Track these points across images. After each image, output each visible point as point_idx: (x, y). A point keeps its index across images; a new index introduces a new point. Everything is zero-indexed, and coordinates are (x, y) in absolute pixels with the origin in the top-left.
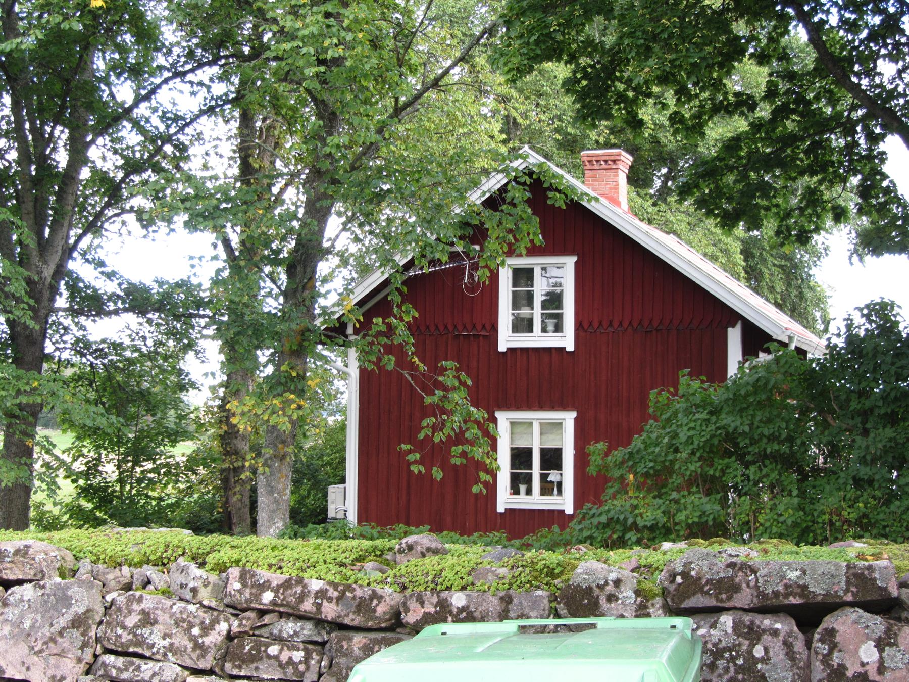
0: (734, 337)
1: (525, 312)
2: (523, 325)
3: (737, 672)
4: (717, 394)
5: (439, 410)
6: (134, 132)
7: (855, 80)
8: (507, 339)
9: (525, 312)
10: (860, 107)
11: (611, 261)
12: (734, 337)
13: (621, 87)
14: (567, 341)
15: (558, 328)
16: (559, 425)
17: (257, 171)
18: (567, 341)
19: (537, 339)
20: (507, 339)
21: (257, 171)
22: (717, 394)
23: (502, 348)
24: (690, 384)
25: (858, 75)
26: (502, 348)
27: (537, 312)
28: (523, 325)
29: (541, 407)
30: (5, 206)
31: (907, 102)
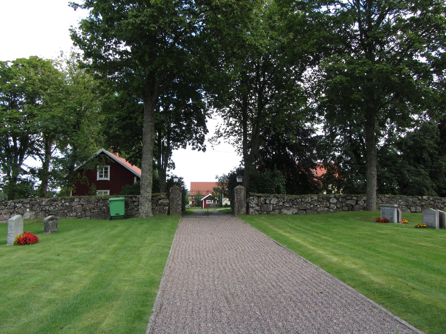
0: (135, 178)
2: (101, 176)
5: (91, 190)
8: (98, 178)
10: (249, 108)
12: (135, 178)
13: (322, 118)
15: (107, 177)
16: (107, 192)
17: (412, 140)
20: (98, 178)
21: (412, 140)
22: (131, 187)
23: (98, 180)
25: (162, 98)
26: (98, 180)
27: (104, 174)
28: (101, 176)
30: (445, 167)
31: (13, 158)
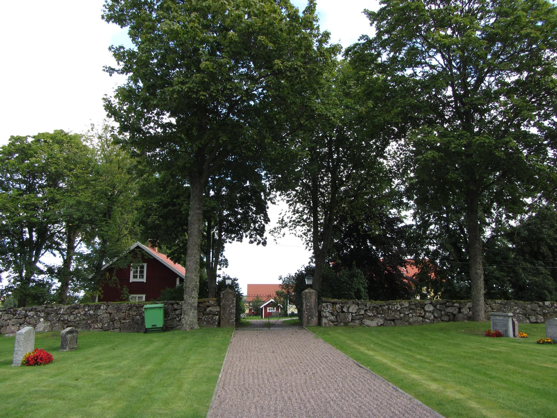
0: (178, 280)
1: (136, 274)
2: (135, 277)
3: (219, 94)
4: (172, 290)
6: (300, 230)
7: (409, 172)
8: (132, 280)
9: (136, 274)
11: (154, 263)
12: (178, 280)
14: (144, 280)
15: (143, 277)
16: (142, 297)
18: (144, 280)
19: (138, 280)
20: (132, 280)
22: (172, 290)
24: (168, 289)
27: (138, 274)
28: (135, 277)
29: (139, 294)
